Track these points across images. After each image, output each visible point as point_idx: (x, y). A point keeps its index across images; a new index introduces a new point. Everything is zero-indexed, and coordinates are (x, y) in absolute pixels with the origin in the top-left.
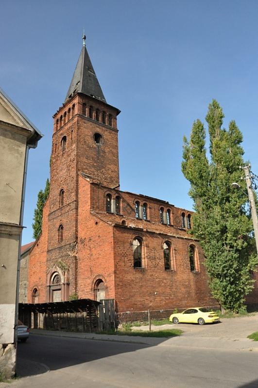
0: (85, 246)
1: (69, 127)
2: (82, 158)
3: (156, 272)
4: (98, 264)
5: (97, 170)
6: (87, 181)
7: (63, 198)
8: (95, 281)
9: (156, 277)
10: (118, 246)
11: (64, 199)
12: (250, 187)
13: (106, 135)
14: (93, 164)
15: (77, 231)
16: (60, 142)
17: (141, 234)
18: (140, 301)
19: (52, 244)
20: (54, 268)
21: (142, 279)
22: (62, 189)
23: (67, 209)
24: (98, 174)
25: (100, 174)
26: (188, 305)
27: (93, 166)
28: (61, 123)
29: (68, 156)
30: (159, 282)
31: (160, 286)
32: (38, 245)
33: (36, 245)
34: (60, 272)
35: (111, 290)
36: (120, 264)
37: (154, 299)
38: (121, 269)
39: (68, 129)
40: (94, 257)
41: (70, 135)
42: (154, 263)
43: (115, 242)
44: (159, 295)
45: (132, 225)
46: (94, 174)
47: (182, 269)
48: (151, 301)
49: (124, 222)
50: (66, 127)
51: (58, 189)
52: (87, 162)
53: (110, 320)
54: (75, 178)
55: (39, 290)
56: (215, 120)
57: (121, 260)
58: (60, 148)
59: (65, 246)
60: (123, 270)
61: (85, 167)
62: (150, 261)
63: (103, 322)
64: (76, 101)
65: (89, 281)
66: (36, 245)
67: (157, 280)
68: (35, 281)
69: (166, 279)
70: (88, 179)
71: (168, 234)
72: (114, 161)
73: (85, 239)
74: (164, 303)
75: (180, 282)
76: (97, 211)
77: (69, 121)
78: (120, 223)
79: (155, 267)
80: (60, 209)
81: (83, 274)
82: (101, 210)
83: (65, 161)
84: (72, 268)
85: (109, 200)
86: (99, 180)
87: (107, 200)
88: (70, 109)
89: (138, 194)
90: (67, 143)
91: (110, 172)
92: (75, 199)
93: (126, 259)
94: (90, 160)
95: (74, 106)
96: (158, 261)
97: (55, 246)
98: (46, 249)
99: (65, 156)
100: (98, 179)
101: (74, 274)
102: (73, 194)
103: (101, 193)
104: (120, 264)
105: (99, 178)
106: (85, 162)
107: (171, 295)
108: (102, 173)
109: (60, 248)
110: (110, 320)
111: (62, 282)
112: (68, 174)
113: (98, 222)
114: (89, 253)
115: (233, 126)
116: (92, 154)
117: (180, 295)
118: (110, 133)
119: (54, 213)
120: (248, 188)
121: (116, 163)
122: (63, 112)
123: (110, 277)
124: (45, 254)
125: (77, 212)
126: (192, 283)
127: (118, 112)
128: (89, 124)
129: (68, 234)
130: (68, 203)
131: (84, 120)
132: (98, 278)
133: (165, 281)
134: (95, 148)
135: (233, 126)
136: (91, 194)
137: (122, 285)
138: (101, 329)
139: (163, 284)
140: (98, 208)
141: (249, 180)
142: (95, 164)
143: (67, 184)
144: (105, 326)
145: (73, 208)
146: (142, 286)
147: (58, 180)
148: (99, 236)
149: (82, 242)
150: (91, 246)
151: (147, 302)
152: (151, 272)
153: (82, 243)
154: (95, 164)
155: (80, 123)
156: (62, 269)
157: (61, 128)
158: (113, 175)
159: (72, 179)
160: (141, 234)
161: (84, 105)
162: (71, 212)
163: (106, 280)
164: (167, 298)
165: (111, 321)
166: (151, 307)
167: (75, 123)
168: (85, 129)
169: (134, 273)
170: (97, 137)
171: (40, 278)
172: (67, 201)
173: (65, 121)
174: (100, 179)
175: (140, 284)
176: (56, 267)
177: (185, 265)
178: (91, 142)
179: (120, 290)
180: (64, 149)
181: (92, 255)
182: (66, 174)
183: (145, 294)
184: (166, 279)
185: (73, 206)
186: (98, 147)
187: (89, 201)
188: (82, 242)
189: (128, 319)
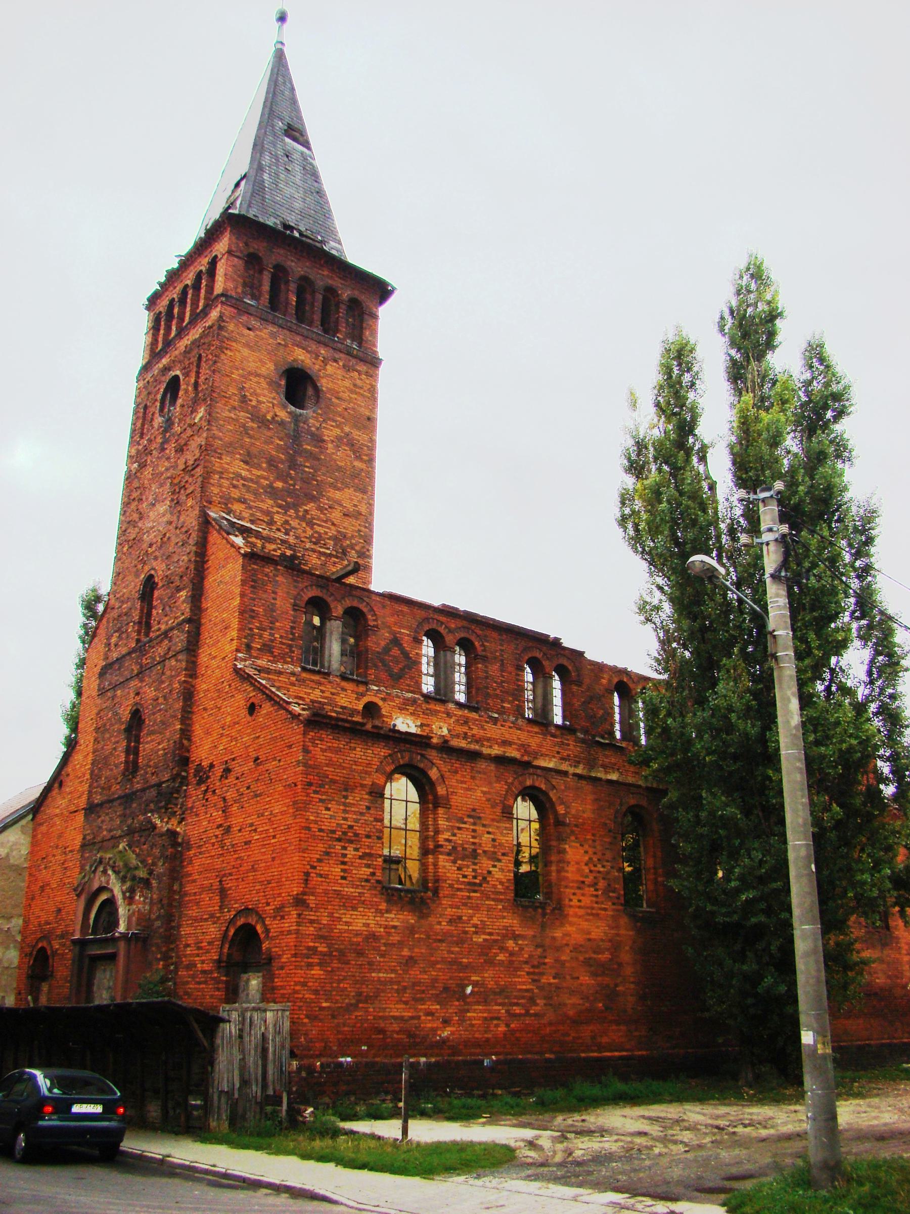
0: (209, 795)
1: (193, 343)
2: (227, 459)
3: (477, 908)
4: (245, 867)
5: (286, 508)
6: (233, 545)
7: (151, 607)
8: (232, 932)
9: (475, 926)
10: (321, 800)
11: (154, 612)
12: (772, 576)
13: (332, 376)
14: (271, 486)
15: (186, 733)
16: (159, 397)
17: (422, 755)
18: (402, 1018)
19: (103, 781)
20: (99, 873)
21: (412, 930)
22: (151, 576)
23: (161, 650)
24: (287, 522)
25: (294, 523)
26: (605, 1040)
27: (272, 492)
28: (168, 329)
29: (180, 450)
30: (486, 948)
31: (491, 962)
32: (474, 810)
33: (56, 785)
34: (117, 889)
35: (282, 968)
36: (324, 868)
37: (462, 1012)
38: (326, 892)
39: (187, 351)
40: (237, 837)
41: (193, 375)
42: (469, 872)
43: (310, 784)
44: (483, 996)
45: (405, 724)
46: (271, 523)
47: (586, 901)
48: (446, 1022)
49: (371, 709)
50: (186, 342)
51: (137, 575)
52: (244, 473)
53: (265, 1087)
54: (194, 535)
55: (55, 953)
56: (752, 333)
57: (328, 854)
58: (159, 420)
59: (143, 790)
60: (338, 893)
61: (235, 494)
62: (454, 862)
63: (229, 1094)
64: (221, 246)
65: (213, 931)
66: (56, 785)
67: (480, 939)
68: (43, 920)
69: (515, 937)
70: (239, 541)
71: (536, 763)
72: (356, 475)
73: (212, 766)
74: (502, 1029)
75: (577, 948)
76: (262, 662)
77: (193, 322)
78: (354, 712)
79: (473, 887)
80: (140, 649)
81: (197, 903)
82: (282, 658)
83: (167, 469)
84: (159, 877)
85: (316, 621)
86: (290, 547)
87: (309, 623)
88: (199, 276)
89: (436, 603)
90: (180, 401)
91: (336, 515)
92: (187, 615)
93: (351, 852)
94: (259, 467)
95: (214, 262)
96: (486, 863)
97: (113, 789)
98: (83, 802)
99: (171, 447)
100: (284, 542)
101: (165, 901)
102: (183, 593)
103: (283, 593)
104: (324, 868)
105: (284, 532)
106: (239, 476)
107: (532, 1000)
108: (303, 518)
109: (127, 799)
110: (265, 1087)
111: (122, 928)
112: (175, 518)
113: (256, 702)
114: (219, 821)
115: (816, 355)
116: (273, 444)
117: (575, 1000)
118: (347, 368)
119: (117, 666)
120: (768, 581)
121: (363, 482)
122: (179, 287)
123: (283, 917)
124: (80, 818)
125: (192, 669)
126: (626, 957)
127: (381, 290)
128: (266, 332)
129: (155, 746)
130: (163, 627)
131: (244, 318)
132: (241, 921)
133: (510, 943)
134: (282, 423)
135: (816, 355)
136: (242, 595)
137: (324, 954)
138: (219, 1123)
139: (501, 957)
140: (267, 649)
141: (772, 547)
142: (279, 484)
143: (169, 557)
144: (240, 1111)
145: (180, 646)
146: (411, 958)
147: (141, 540)
148: (257, 759)
149: (203, 775)
150: (229, 795)
151: (428, 1024)
152: (451, 906)
153: (201, 782)
154: (279, 484)
155: (231, 327)
156: (123, 880)
157: (168, 344)
158: (349, 527)
159: (184, 537)
160: (422, 755)
161: (252, 261)
162: (173, 662)
163: (267, 931)
164: (517, 1010)
165: (270, 1092)
166: (444, 1041)
167: (210, 327)
168: (246, 352)
169: (383, 906)
170: (297, 385)
171: (59, 910)
172: (162, 621)
173: (181, 318)
174: (292, 540)
175: (406, 952)
176: (105, 872)
177: (602, 884)
178: (270, 401)
179: (316, 971)
180: (169, 423)
181: (228, 830)
182: (168, 517)
183: (423, 992)
184: (515, 937)
185: (180, 639)
186: (296, 419)
187: (235, 624)
188: (203, 775)
189: (343, 1087)
